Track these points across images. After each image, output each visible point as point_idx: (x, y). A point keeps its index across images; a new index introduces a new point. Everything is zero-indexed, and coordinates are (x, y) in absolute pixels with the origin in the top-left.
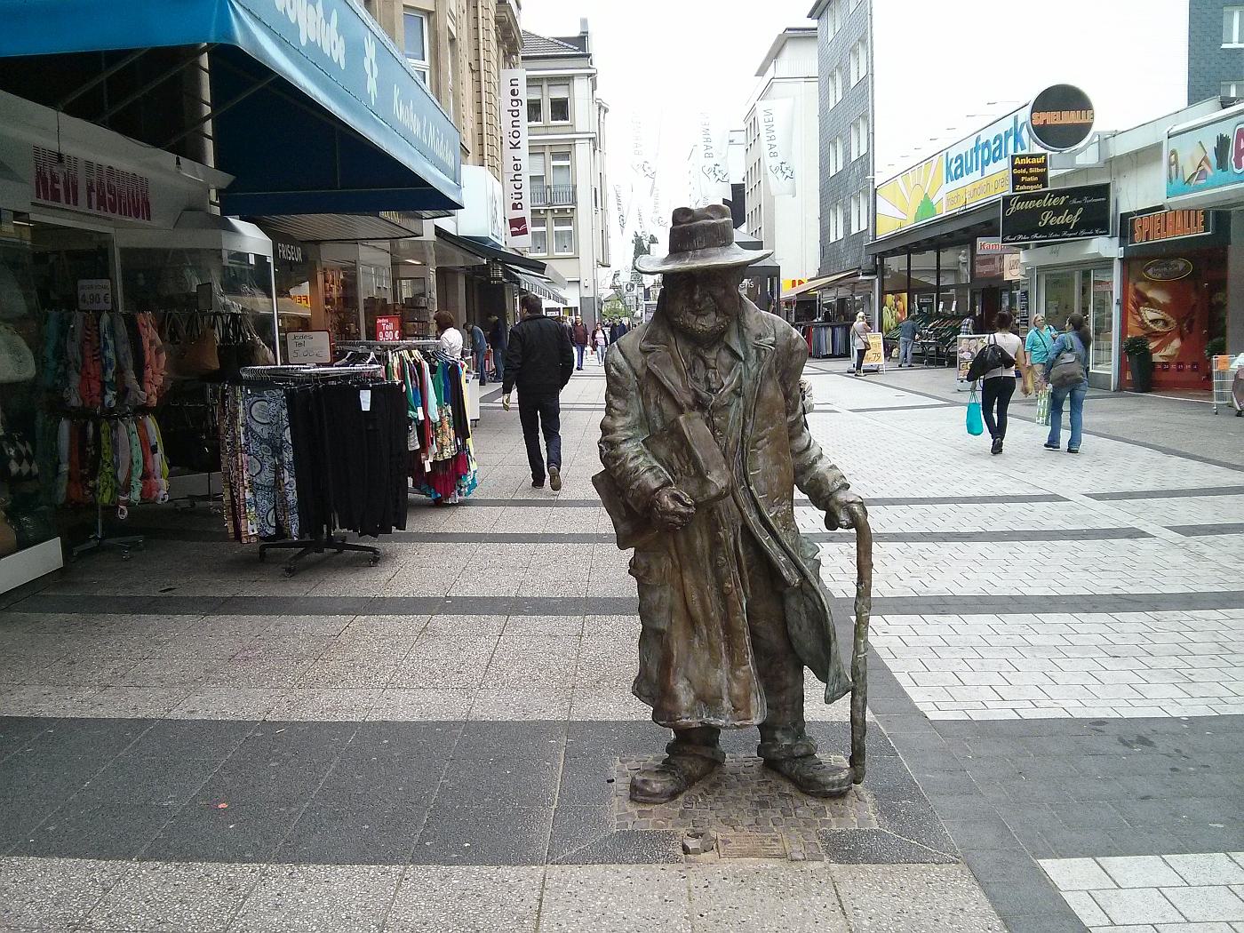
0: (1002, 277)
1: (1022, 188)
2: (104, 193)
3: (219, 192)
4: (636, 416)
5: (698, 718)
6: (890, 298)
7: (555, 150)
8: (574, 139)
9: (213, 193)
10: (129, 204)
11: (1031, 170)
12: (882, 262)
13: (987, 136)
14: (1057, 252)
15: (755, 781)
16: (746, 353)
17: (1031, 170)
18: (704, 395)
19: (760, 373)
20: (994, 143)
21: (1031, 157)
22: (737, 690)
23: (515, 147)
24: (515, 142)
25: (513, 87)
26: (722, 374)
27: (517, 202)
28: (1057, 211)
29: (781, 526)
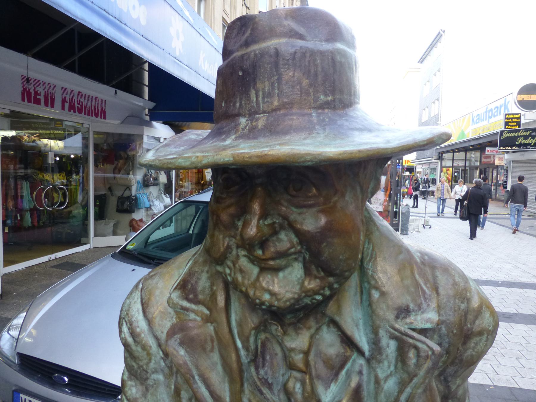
0: (494, 164)
1: (509, 127)
2: (74, 104)
3: (149, 110)
6: (445, 169)
9: (147, 110)
11: (513, 120)
12: (442, 155)
13: (493, 106)
14: (523, 155)
16: (375, 343)
17: (513, 120)
20: (494, 109)
21: (514, 114)
26: (319, 377)
28: (526, 137)
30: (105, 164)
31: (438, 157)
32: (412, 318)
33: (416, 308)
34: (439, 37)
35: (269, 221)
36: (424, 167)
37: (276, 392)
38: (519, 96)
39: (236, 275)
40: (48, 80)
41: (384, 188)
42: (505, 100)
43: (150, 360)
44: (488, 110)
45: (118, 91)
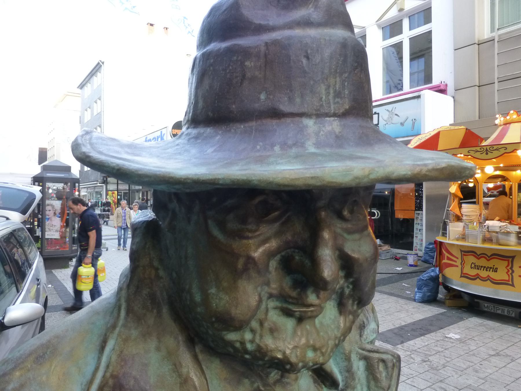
6: (110, 193)
12: (107, 178)
31: (103, 181)
34: (98, 68)
36: (89, 191)
38: (173, 130)
39: (264, 338)
41: (60, 214)
42: (161, 132)
44: (147, 139)
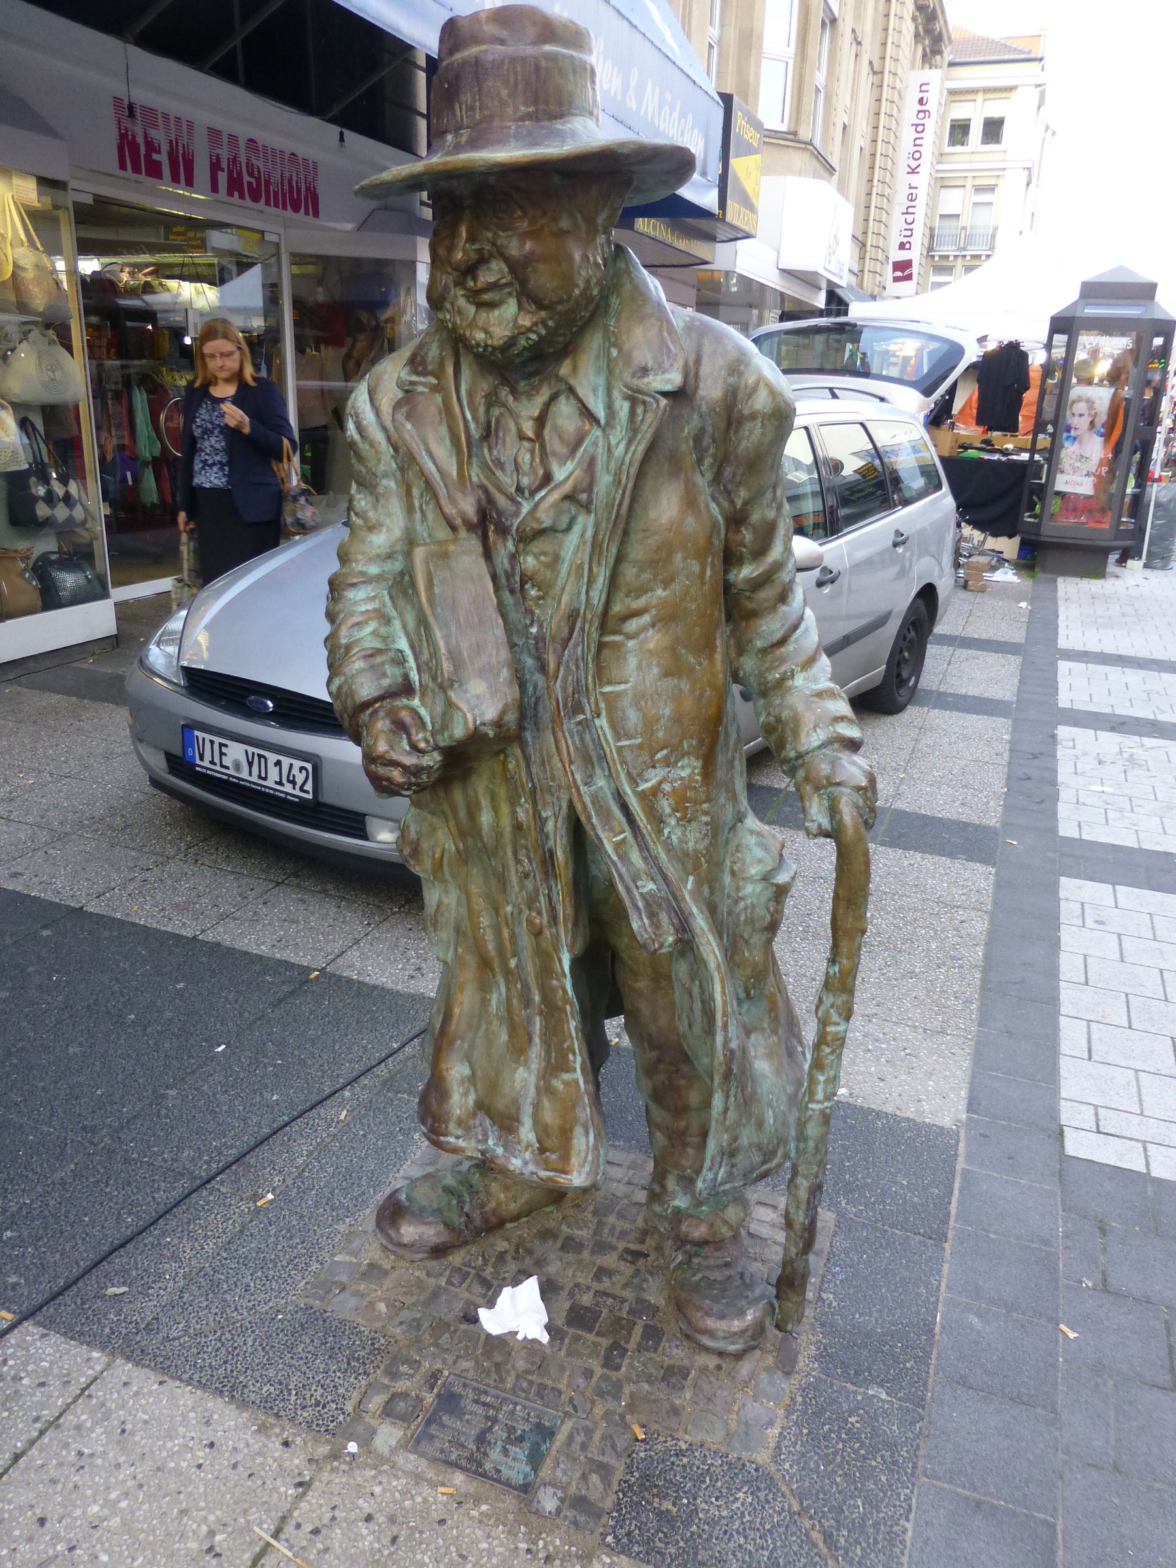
2: (240, 174)
4: (397, 533)
5: (479, 1141)
7: (978, 182)
8: (1004, 169)
10: (284, 195)
15: (621, 1245)
18: (502, 501)
19: (627, 459)
22: (549, 1116)
23: (913, 171)
24: (914, 164)
25: (922, 95)
26: (554, 454)
27: (905, 240)
29: (668, 810)
30: (322, 347)
32: (651, 378)
33: (656, 367)
35: (477, 246)
37: (509, 473)
40: (174, 107)
43: (379, 460)
45: (347, 133)
